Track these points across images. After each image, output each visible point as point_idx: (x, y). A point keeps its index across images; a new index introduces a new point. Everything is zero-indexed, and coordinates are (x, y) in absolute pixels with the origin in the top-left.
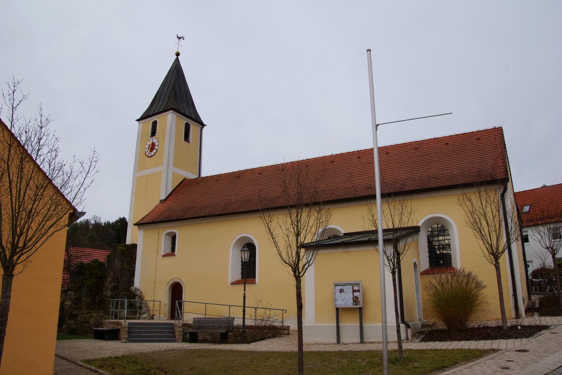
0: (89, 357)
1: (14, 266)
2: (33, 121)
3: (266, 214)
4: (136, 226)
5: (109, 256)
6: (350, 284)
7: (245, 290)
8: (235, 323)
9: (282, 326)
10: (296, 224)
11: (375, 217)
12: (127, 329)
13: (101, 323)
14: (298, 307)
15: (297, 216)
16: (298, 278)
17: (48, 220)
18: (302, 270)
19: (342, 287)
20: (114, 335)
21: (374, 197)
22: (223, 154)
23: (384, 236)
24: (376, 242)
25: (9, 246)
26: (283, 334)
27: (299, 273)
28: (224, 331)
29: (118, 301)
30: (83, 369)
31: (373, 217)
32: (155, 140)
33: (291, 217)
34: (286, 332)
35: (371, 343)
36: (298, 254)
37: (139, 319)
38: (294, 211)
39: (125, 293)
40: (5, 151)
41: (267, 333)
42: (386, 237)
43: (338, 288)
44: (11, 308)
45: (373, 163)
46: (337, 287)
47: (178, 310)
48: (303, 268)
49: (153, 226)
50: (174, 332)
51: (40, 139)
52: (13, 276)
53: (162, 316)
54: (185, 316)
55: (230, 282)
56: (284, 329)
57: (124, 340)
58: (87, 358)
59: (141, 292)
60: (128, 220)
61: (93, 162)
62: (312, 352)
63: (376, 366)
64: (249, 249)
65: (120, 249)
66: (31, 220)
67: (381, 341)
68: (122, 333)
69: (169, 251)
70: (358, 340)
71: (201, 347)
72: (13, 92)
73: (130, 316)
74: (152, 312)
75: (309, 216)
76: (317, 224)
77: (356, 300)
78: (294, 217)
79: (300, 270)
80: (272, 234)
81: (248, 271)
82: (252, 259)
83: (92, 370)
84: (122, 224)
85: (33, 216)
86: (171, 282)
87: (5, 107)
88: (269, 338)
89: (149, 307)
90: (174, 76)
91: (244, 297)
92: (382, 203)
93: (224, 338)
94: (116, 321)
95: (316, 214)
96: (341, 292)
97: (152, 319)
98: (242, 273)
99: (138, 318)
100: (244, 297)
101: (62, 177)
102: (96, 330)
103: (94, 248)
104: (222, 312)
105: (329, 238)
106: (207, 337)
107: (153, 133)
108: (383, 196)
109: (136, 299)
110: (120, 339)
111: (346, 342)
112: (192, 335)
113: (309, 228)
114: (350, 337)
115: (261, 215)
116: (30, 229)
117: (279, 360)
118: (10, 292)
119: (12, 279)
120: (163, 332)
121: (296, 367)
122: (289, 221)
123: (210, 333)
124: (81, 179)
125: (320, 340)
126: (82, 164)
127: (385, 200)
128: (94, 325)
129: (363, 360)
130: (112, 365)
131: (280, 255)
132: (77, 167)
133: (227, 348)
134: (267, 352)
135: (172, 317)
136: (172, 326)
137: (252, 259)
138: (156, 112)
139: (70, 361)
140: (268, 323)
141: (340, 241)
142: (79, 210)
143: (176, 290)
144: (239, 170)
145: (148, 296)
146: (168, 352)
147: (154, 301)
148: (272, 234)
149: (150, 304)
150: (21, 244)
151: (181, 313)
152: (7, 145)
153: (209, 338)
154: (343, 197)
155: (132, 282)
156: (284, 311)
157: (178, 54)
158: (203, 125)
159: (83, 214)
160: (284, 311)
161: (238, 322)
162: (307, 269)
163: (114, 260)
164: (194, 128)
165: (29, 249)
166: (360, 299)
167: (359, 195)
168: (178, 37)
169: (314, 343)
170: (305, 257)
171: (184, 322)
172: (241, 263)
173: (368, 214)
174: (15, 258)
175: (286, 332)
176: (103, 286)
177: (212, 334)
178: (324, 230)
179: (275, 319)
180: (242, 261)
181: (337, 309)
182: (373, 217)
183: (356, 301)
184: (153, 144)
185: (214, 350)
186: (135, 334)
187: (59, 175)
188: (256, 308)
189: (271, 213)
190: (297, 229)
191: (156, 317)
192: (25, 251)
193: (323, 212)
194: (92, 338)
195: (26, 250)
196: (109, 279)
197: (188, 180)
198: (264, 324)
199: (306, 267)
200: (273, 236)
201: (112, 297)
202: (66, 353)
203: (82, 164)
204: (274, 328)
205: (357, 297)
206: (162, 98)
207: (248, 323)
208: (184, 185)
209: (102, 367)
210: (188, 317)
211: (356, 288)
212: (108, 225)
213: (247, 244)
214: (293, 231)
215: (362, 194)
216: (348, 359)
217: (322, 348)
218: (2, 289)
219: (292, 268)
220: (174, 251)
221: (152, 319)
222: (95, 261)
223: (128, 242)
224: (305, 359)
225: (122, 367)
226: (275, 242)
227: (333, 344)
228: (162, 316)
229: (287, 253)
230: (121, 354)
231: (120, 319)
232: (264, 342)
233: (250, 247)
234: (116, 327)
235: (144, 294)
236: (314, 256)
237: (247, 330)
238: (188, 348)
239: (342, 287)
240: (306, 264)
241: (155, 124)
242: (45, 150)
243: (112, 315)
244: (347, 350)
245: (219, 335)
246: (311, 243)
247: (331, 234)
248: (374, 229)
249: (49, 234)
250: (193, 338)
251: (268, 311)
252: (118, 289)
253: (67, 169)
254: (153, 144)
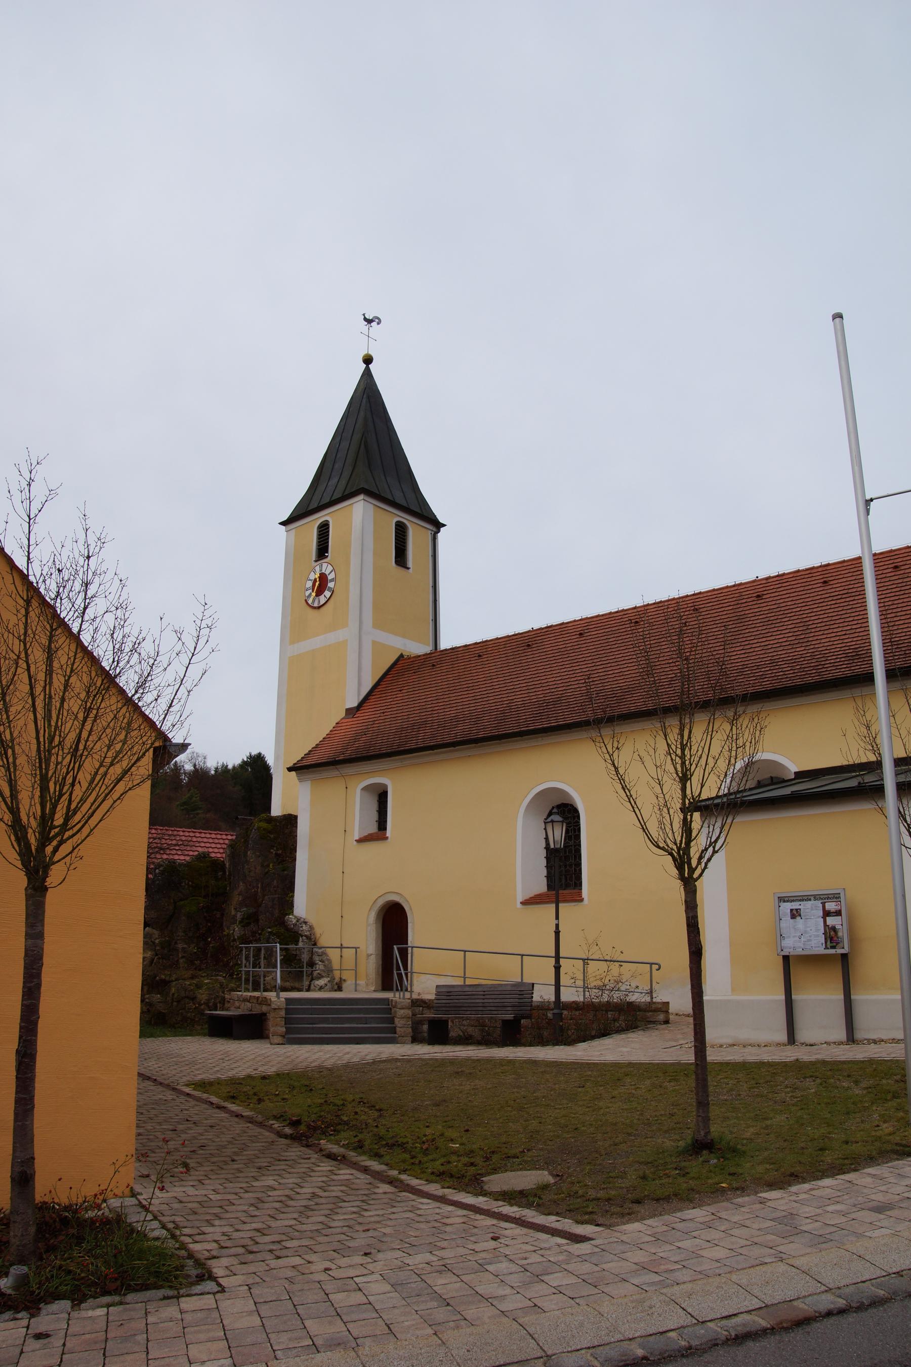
0: (203, 1076)
1: (46, 868)
2: (69, 544)
3: (607, 732)
4: (294, 773)
5: (232, 846)
6: (816, 897)
7: (557, 918)
8: (536, 998)
9: (651, 1003)
10: (679, 752)
11: (873, 729)
12: (283, 1013)
13: (223, 1001)
14: (692, 953)
15: (682, 735)
16: (689, 884)
17: (112, 764)
18: (699, 863)
19: (795, 905)
20: (252, 1027)
21: (868, 678)
22: (488, 593)
23: (897, 774)
24: (878, 791)
25: (34, 824)
26: (654, 1022)
27: (692, 870)
28: (510, 1017)
29: (259, 949)
30: (193, 1103)
31: (868, 727)
32: (327, 568)
33: (665, 736)
34: (661, 1017)
35: (875, 1042)
36: (687, 827)
37: (308, 990)
38: (673, 722)
39: (275, 930)
40: (20, 616)
41: (615, 1020)
42: (902, 778)
43: (787, 907)
44: (46, 960)
45: (862, 593)
46: (783, 905)
47: (398, 969)
48: (701, 858)
49: (332, 772)
50: (391, 1020)
51: (86, 585)
52: (46, 889)
53: (362, 984)
54: (415, 982)
55: (520, 898)
56: (657, 1010)
57: (277, 1039)
58: (200, 1077)
59: (311, 927)
60: (270, 760)
61: (204, 628)
62: (727, 1064)
63: (889, 1096)
64: (565, 818)
65: (259, 828)
66: (77, 765)
67: (901, 1037)
68: (270, 1023)
69: (373, 828)
70: (842, 1035)
71: (458, 1054)
72: (29, 485)
73: (288, 984)
74: (337, 974)
75: (710, 732)
76: (730, 750)
77: (831, 936)
78: (673, 736)
79: (694, 863)
80: (621, 780)
81: (563, 872)
82: (572, 843)
83: (212, 1103)
84: (256, 771)
85: (82, 755)
86: (381, 902)
87: (13, 517)
88: (619, 1031)
89: (330, 961)
90: (362, 414)
91: (557, 933)
92: (889, 692)
93: (511, 1034)
94: (256, 994)
95: (727, 727)
96: (793, 916)
97: (340, 989)
98: (549, 877)
99: (305, 987)
100: (557, 933)
101: (138, 668)
102: (212, 1017)
103: (193, 826)
104: (506, 972)
105: (760, 785)
106: (470, 1029)
107: (322, 551)
108: (891, 675)
109: (301, 944)
110: (267, 1037)
111: (809, 1041)
112: (437, 1022)
113: (711, 762)
114: (821, 1027)
115: (594, 734)
116: (77, 787)
117: (648, 1082)
118: (43, 926)
119: (44, 896)
120: (366, 1021)
121: (692, 1099)
122: (662, 746)
123: (478, 1020)
124: (178, 668)
125: (744, 1035)
126: (179, 634)
127: (897, 685)
128: (207, 1004)
129: (856, 1082)
130: (255, 1094)
131: (644, 829)
132: (168, 642)
133: (520, 1054)
134: (616, 1065)
135: (386, 983)
136: (387, 1007)
137: (572, 843)
138: (326, 500)
139: (161, 1084)
140: (616, 997)
141: (787, 791)
142: (177, 737)
143: (393, 921)
144: (528, 628)
145: (327, 937)
146: (382, 1066)
147: (341, 947)
148: (621, 780)
149: (334, 955)
150: (59, 820)
151: (406, 975)
152: (21, 602)
153: (475, 1032)
154: (789, 683)
155: (288, 905)
156: (655, 967)
157: (368, 360)
158: (438, 525)
159: (184, 747)
160: (655, 967)
161: (543, 994)
162: (709, 860)
163: (246, 855)
164: (416, 533)
165: (76, 829)
166: (843, 933)
167: (829, 676)
168: (365, 319)
169: (730, 1041)
170: (705, 831)
171: (415, 996)
172: (544, 853)
173: (857, 723)
174: (49, 849)
175: (661, 1017)
176: (222, 915)
177: (481, 1024)
178: (749, 765)
179: (634, 985)
180: (547, 847)
181: (786, 958)
182: (868, 727)
183: (832, 939)
184: (323, 578)
185: (488, 1060)
186: (303, 1025)
187: (132, 663)
188: (585, 961)
189: (618, 730)
190: (683, 763)
191: (348, 985)
192: (67, 834)
193: (744, 721)
194: (205, 1035)
195: (70, 833)
196: (236, 899)
197: (409, 658)
198: (605, 998)
199: (707, 856)
200: (621, 786)
201: (245, 940)
202: (152, 1067)
203: (179, 634)
204: (632, 1007)
205: (834, 929)
206: (338, 466)
207: (568, 996)
208: (400, 670)
209: (233, 1097)
210: (424, 984)
211: (831, 906)
212: (224, 772)
213: (558, 807)
214: (672, 770)
215: (838, 674)
216: (818, 1081)
217: (751, 1055)
218: (27, 919)
219: (674, 859)
220: (385, 829)
221: (340, 989)
222: (203, 857)
223: (276, 810)
224: (711, 1082)
225: (279, 1098)
226: (629, 797)
227: (778, 1044)
228: (362, 982)
229: (661, 823)
230: (274, 1069)
231: (265, 990)
232: (607, 1042)
233: (566, 813)
234: (257, 1009)
235: (318, 931)
236: (726, 828)
237: (565, 1012)
238: (427, 1056)
239: (795, 905)
240: (706, 849)
241: (324, 530)
242: (97, 608)
243: (247, 980)
244: (813, 1058)
245: (499, 1024)
246: (717, 797)
247: (765, 775)
248: (873, 758)
249: (115, 795)
250: (438, 1033)
251: (615, 967)
252: (257, 921)
253: (147, 648)
254: (323, 578)
